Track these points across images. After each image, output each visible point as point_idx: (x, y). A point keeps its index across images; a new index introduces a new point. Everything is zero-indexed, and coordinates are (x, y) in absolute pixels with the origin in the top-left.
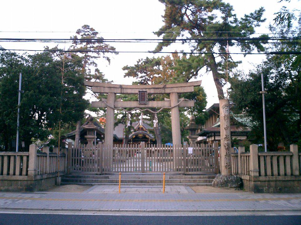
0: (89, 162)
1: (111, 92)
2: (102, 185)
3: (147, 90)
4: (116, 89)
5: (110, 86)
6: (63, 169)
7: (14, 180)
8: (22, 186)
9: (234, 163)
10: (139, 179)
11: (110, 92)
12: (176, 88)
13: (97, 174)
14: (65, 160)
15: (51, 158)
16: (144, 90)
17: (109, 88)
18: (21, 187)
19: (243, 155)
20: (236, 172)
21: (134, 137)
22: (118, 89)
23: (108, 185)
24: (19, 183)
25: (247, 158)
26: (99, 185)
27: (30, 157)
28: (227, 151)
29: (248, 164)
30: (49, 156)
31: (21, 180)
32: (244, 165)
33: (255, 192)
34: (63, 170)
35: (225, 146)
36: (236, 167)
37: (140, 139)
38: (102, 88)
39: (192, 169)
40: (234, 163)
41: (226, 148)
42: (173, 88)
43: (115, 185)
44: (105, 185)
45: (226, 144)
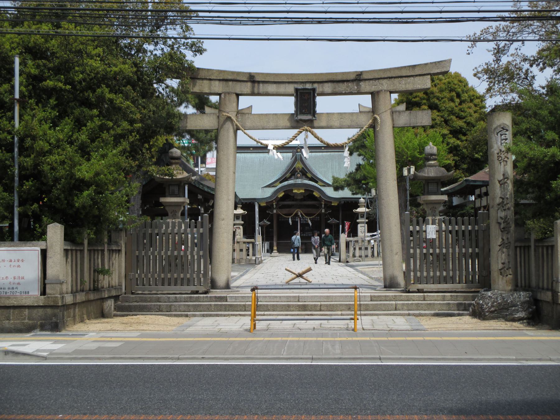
0: (173, 264)
1: (227, 90)
2: (210, 316)
3: (316, 86)
4: (239, 84)
5: (226, 78)
6: (117, 281)
7: (15, 307)
8: (33, 319)
9: (523, 264)
10: (299, 301)
11: (224, 91)
12: (385, 81)
13: (197, 292)
14: (373, 288)
15: (92, 255)
16: (308, 86)
17: (221, 82)
18: (30, 322)
19: (540, 245)
20: (527, 282)
21: (281, 195)
22: (243, 84)
23: (225, 316)
24: (26, 312)
25: (550, 252)
26: (203, 316)
27: (49, 254)
28: (502, 236)
29: (527, 265)
30: (88, 250)
31: (29, 307)
32: (543, 267)
33: (529, 324)
34: (117, 284)
35: (499, 224)
36: (527, 273)
37: (296, 200)
38: (205, 81)
39: (176, 280)
40: (523, 264)
41: (502, 226)
42: (381, 81)
43: (240, 315)
44: (217, 315)
45: (501, 218)
